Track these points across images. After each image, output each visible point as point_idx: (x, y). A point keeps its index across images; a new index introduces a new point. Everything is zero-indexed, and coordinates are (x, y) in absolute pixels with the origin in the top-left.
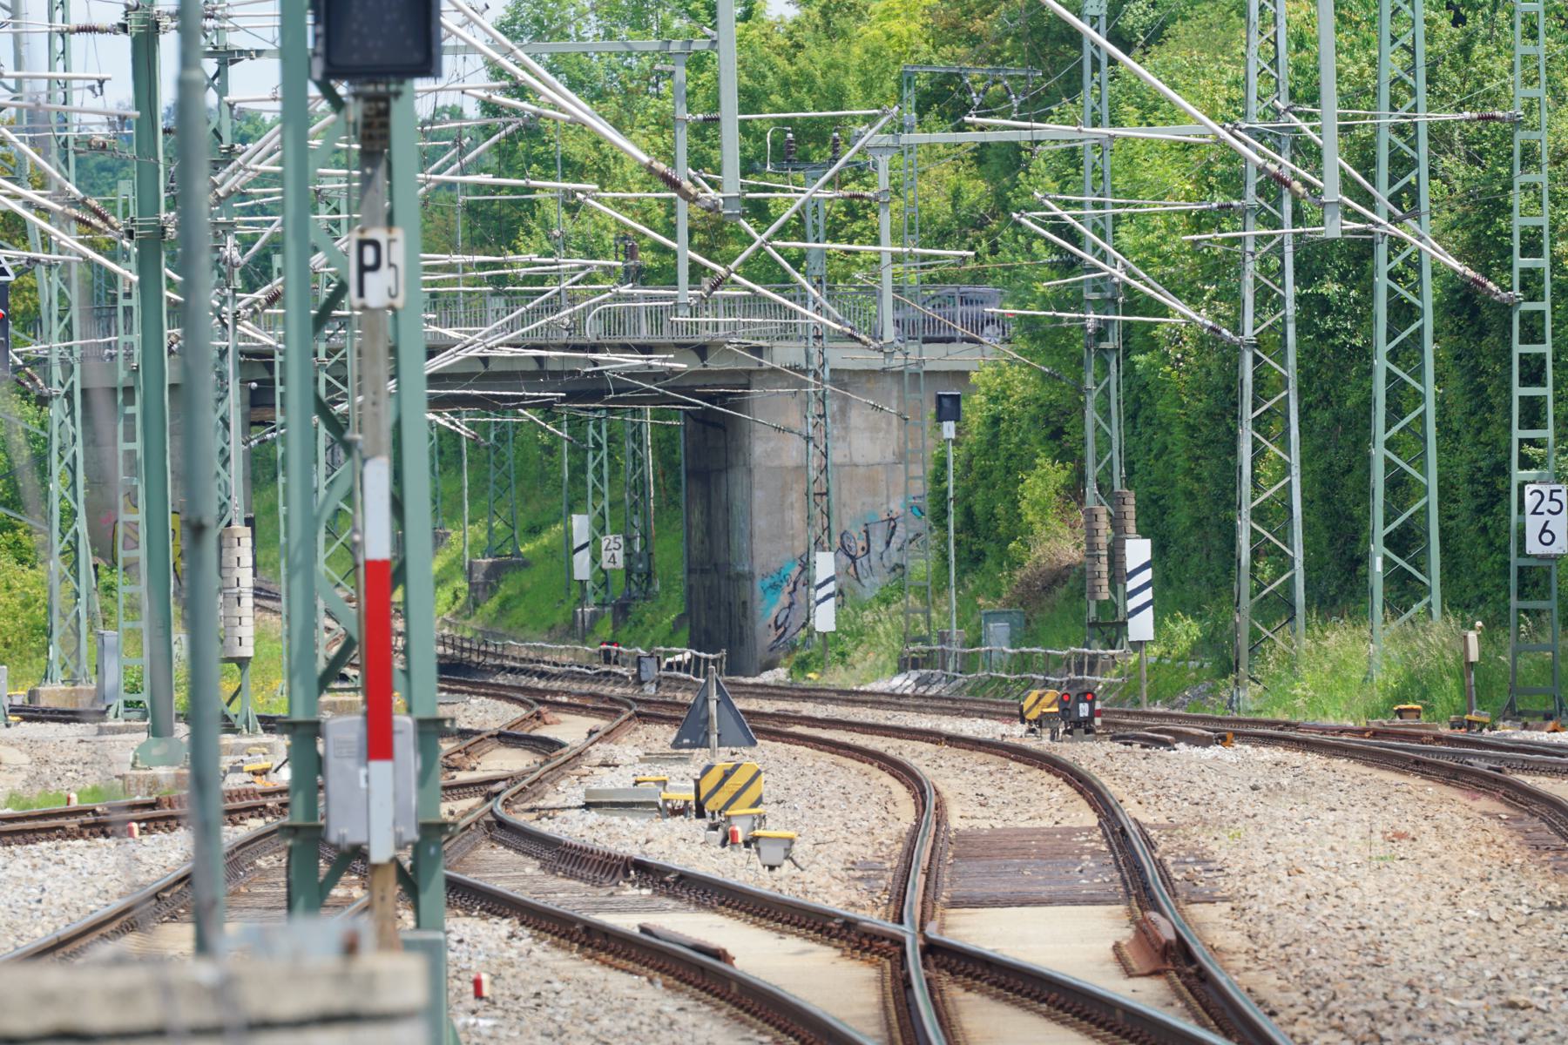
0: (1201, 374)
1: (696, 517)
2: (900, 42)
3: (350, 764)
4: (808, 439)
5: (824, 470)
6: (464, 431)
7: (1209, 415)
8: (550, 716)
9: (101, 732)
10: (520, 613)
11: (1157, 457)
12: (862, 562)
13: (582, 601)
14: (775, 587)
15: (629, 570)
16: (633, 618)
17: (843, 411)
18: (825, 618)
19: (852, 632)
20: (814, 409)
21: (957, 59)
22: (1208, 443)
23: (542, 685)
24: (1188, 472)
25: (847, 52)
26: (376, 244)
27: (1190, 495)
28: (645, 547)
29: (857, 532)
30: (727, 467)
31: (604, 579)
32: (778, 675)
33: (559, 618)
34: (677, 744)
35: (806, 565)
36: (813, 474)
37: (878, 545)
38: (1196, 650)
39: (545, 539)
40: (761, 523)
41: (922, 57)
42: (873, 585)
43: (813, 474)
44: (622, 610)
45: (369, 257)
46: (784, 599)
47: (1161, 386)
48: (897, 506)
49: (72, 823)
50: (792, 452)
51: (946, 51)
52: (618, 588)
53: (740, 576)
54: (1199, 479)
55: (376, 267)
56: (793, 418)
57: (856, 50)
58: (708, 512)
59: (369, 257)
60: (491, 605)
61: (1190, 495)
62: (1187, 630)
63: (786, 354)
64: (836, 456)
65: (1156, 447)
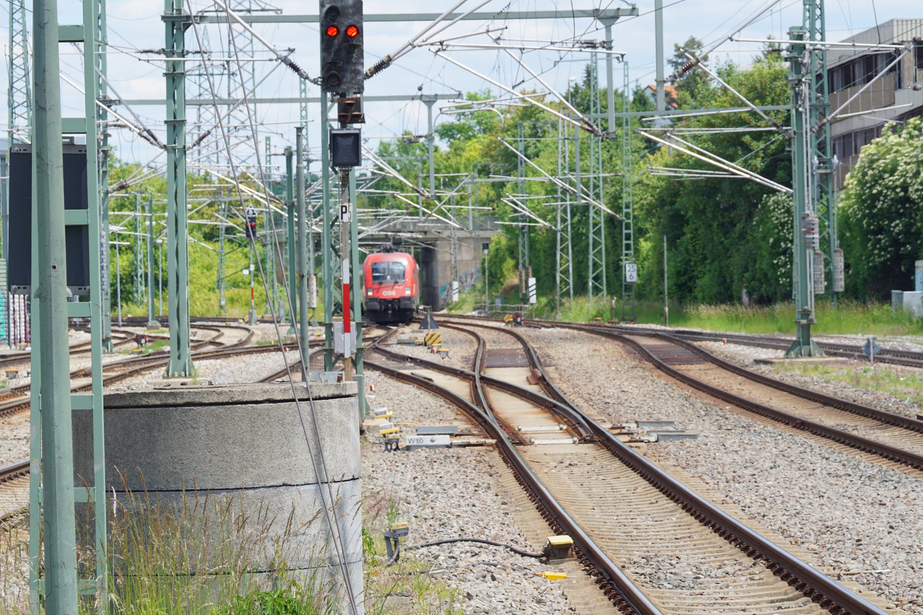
14: (444, 290)
18: (456, 298)
29: (464, 277)
35: (451, 285)
37: (469, 280)
38: (546, 305)
40: (440, 274)
61: (545, 268)
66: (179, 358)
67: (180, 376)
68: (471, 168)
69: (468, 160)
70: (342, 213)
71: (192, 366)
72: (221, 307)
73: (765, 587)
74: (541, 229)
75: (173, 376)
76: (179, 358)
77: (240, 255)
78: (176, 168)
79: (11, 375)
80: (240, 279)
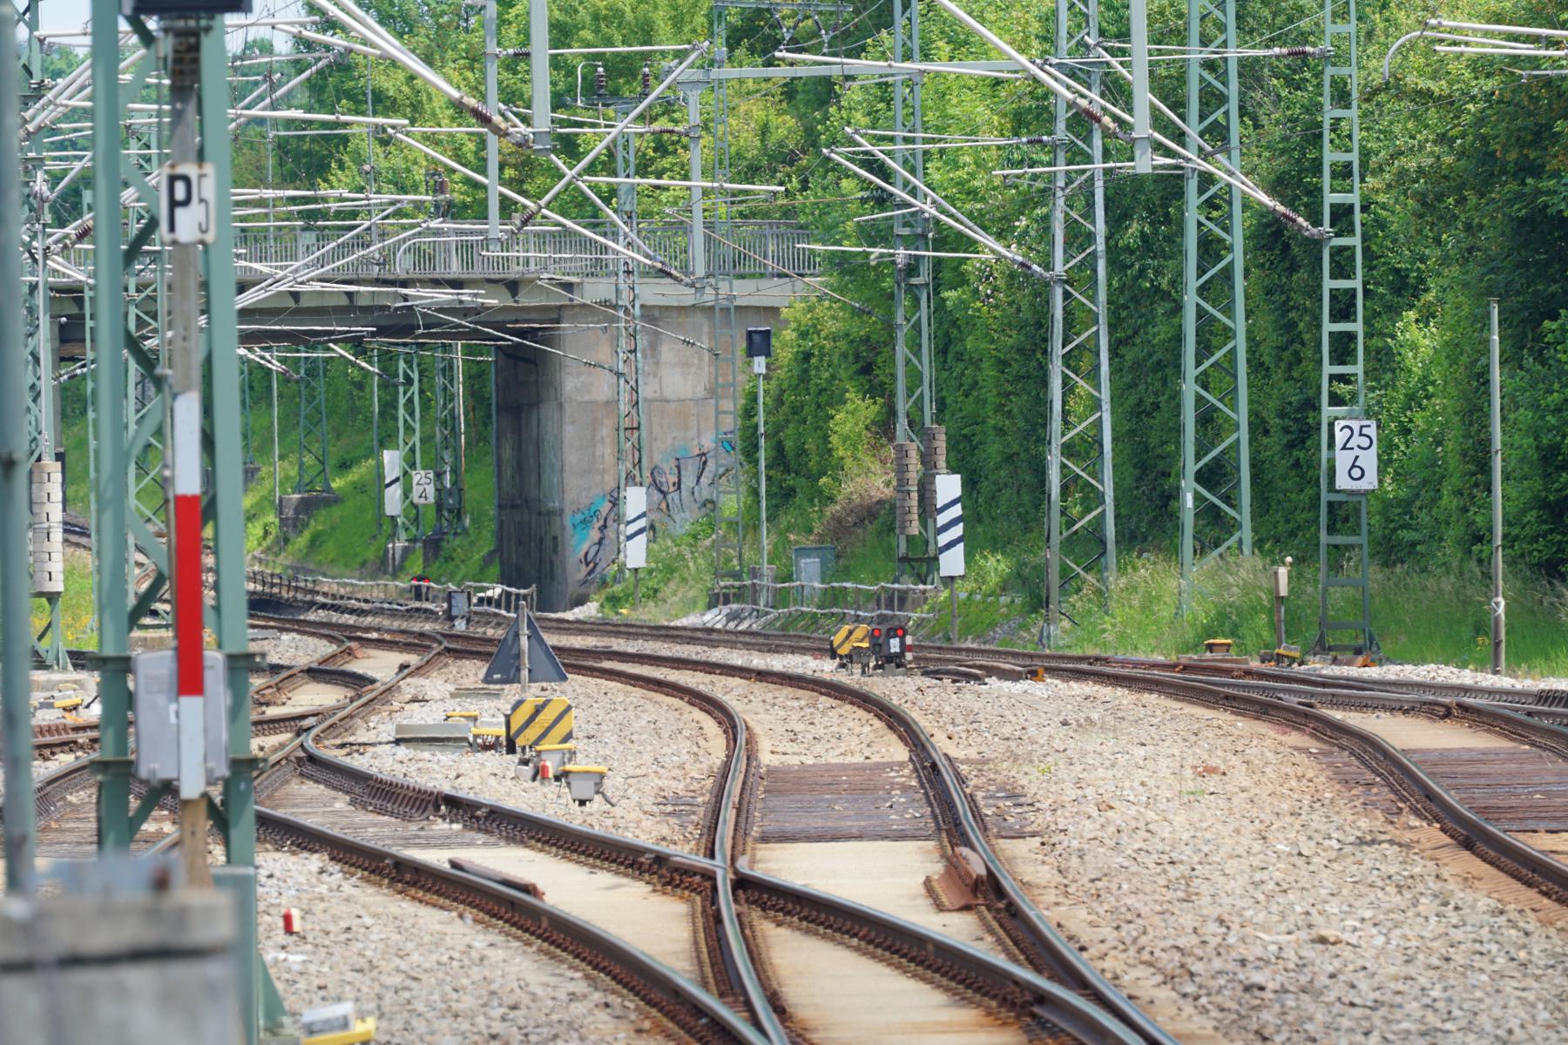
1: (508, 452)
6: (276, 366)
7: (1020, 351)
12: (673, 496)
13: (393, 537)
15: (439, 506)
17: (654, 346)
18: (636, 554)
22: (1019, 378)
26: (186, 180)
27: (1000, 431)
28: (455, 483)
29: (668, 466)
31: (414, 513)
32: (589, 611)
33: (370, 554)
34: (488, 679)
36: (624, 408)
37: (689, 481)
38: (1004, 587)
40: (571, 458)
44: (433, 546)
45: (180, 193)
46: (595, 535)
47: (971, 322)
48: (708, 442)
50: (603, 386)
53: (550, 513)
54: (1009, 414)
55: (186, 202)
56: (603, 354)
58: (519, 447)
59: (180, 193)
60: (302, 541)
61: (1000, 431)
62: (996, 565)
63: (596, 291)
65: (967, 381)
70: (173, 204)
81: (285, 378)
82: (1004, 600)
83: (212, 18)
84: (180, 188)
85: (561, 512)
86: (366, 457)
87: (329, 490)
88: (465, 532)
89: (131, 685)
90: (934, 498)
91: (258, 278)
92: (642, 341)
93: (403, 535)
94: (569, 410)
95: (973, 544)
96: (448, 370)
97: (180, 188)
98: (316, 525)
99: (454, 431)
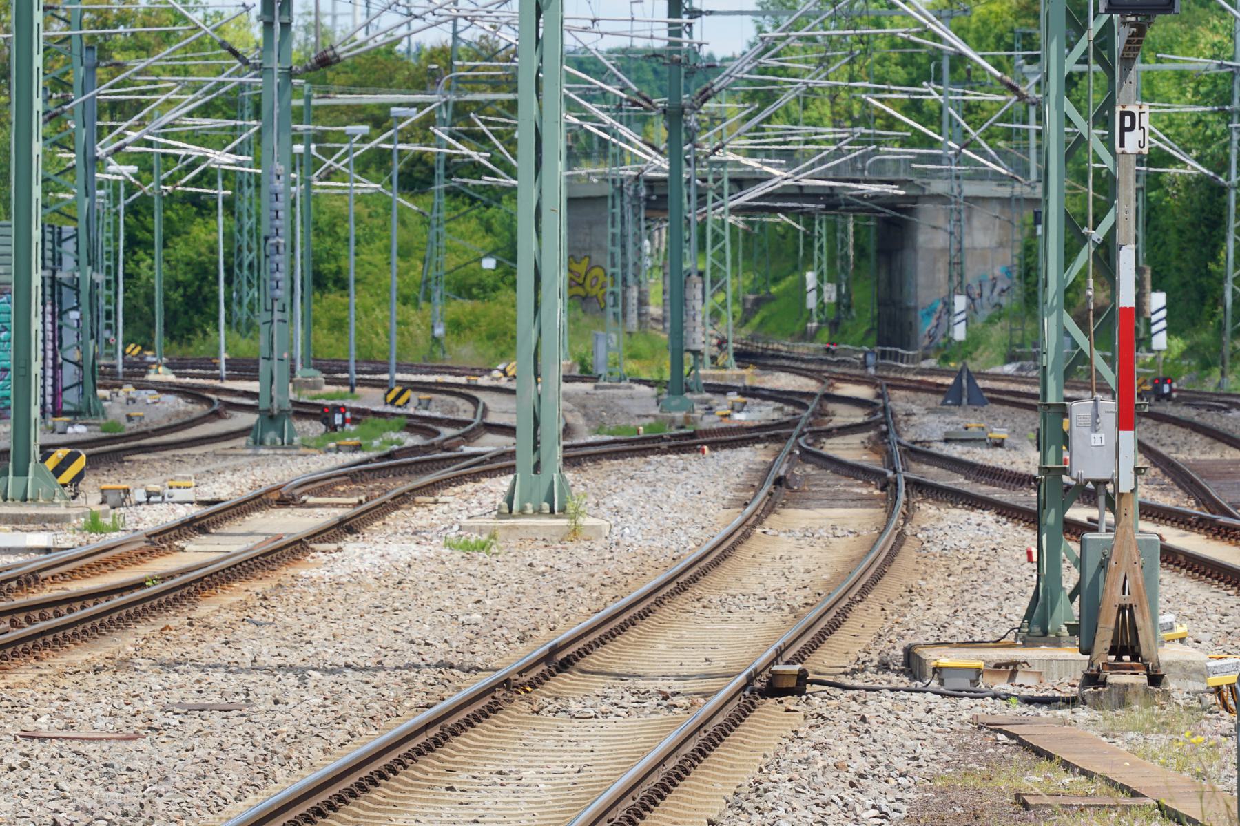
0: (1188, 202)
1: (883, 275)
2: (997, 17)
3: (1086, 431)
4: (951, 233)
5: (960, 250)
6: (741, 226)
7: (1192, 224)
8: (838, 385)
9: (596, 388)
10: (772, 325)
11: (1159, 248)
12: (978, 301)
13: (809, 319)
14: (929, 314)
15: (838, 304)
16: (840, 329)
17: (969, 218)
18: (960, 333)
19: (974, 340)
20: (955, 216)
21: (1028, 25)
22: (1190, 241)
23: (803, 366)
24: (1179, 257)
25: (969, 21)
26: (1131, 114)
27: (1179, 270)
28: (848, 290)
29: (975, 285)
30: (902, 248)
31: (822, 307)
32: (932, 363)
33: (797, 328)
34: (944, 403)
36: (953, 253)
37: (986, 293)
38: (1184, 355)
39: (783, 285)
40: (922, 279)
41: (1009, 25)
42: (985, 313)
43: (953, 253)
44: (835, 325)
45: (1128, 124)
46: (934, 322)
47: (1164, 209)
49: (664, 445)
51: (1022, 21)
52: (831, 314)
53: (908, 309)
54: (1185, 260)
55: (1131, 129)
56: (941, 222)
57: (974, 19)
59: (1128, 124)
61: (1179, 270)
63: (938, 187)
64: (966, 243)
65: (1159, 241)
66: (537, 468)
67: (538, 512)
68: (991, 40)
69: (985, 23)
70: (1123, 130)
71: (565, 487)
72: (436, 340)
73: (656, 779)
74: (1173, 183)
75: (522, 512)
76: (537, 468)
77: (474, 224)
78: (539, 13)
79: (112, 498)
80: (474, 280)
81: (746, 232)
82: (1185, 362)
83: (1149, 17)
84: (1128, 119)
85: (916, 308)
86: (790, 273)
87: (769, 293)
88: (853, 318)
89: (1066, 427)
90: (1146, 308)
91: (764, 176)
92: (964, 215)
93: (815, 318)
94: (920, 254)
95: (1171, 331)
96: (845, 230)
97: (1128, 119)
98: (763, 313)
99: (848, 261)
